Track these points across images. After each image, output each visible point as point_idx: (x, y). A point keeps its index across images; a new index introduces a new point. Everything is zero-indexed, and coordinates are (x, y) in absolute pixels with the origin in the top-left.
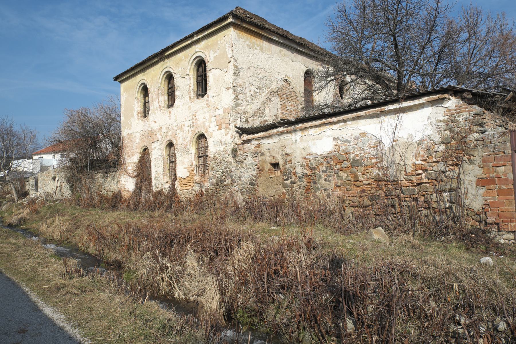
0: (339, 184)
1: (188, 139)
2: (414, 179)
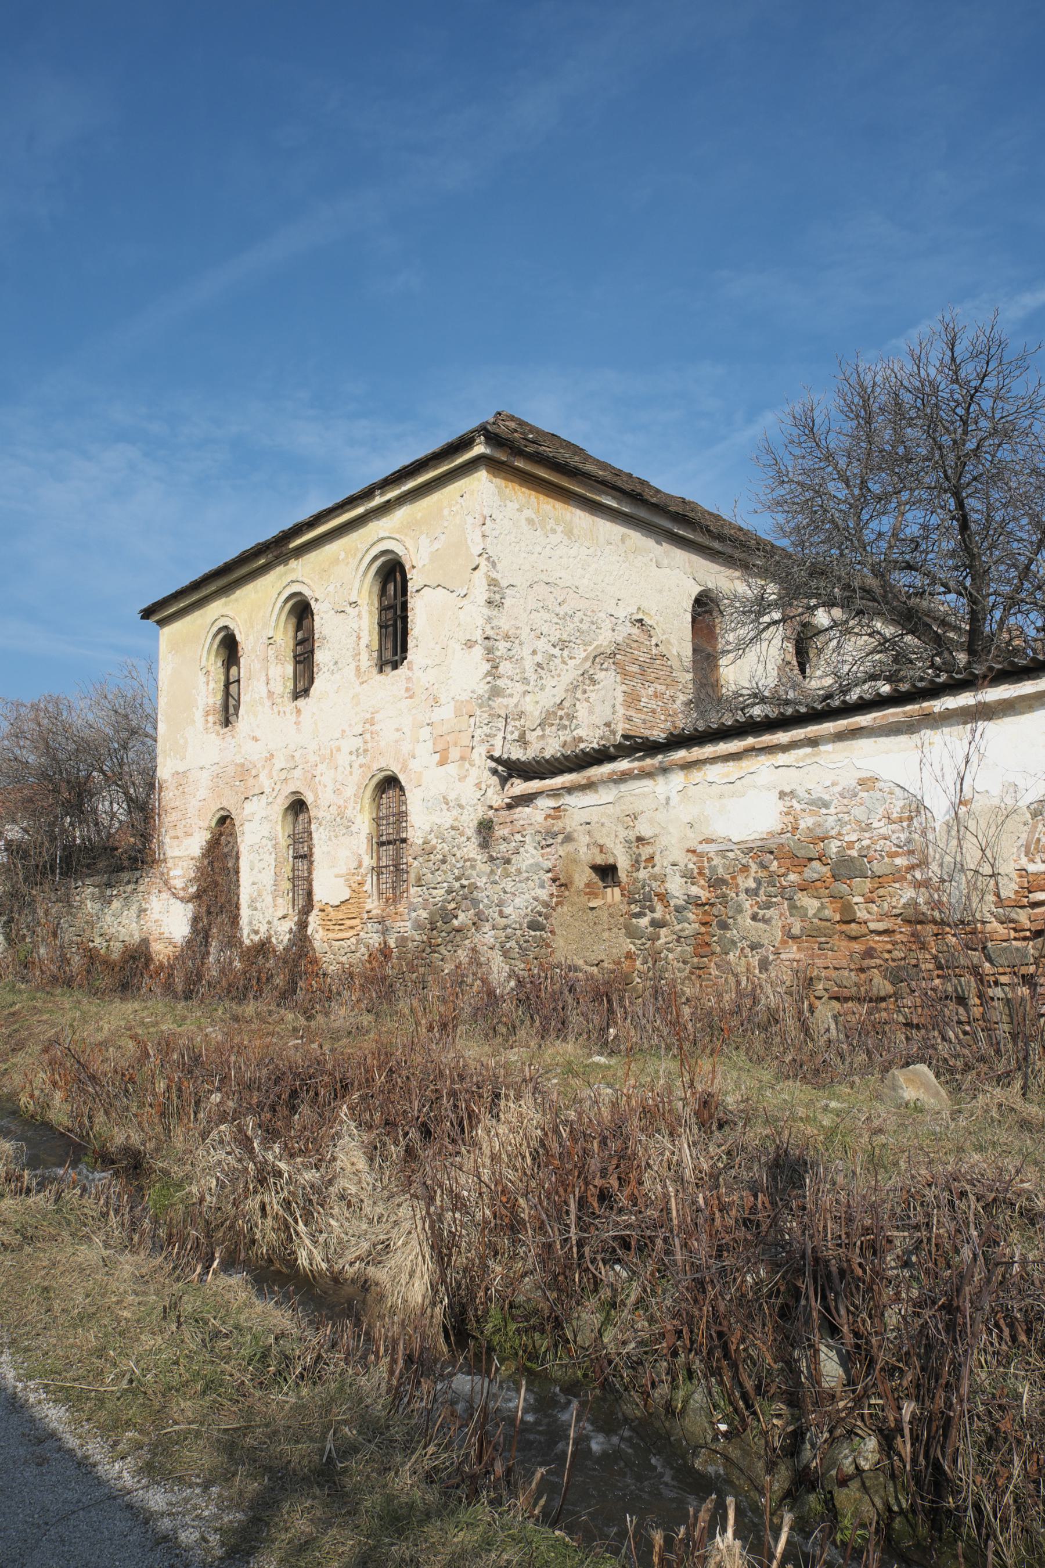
1: (349, 792)
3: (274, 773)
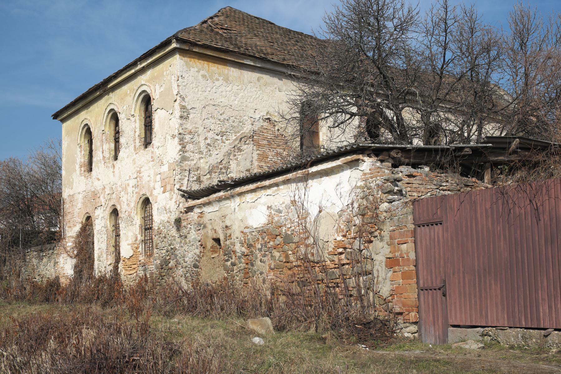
0: (272, 266)
1: (132, 205)
2: (336, 258)
3: (106, 196)
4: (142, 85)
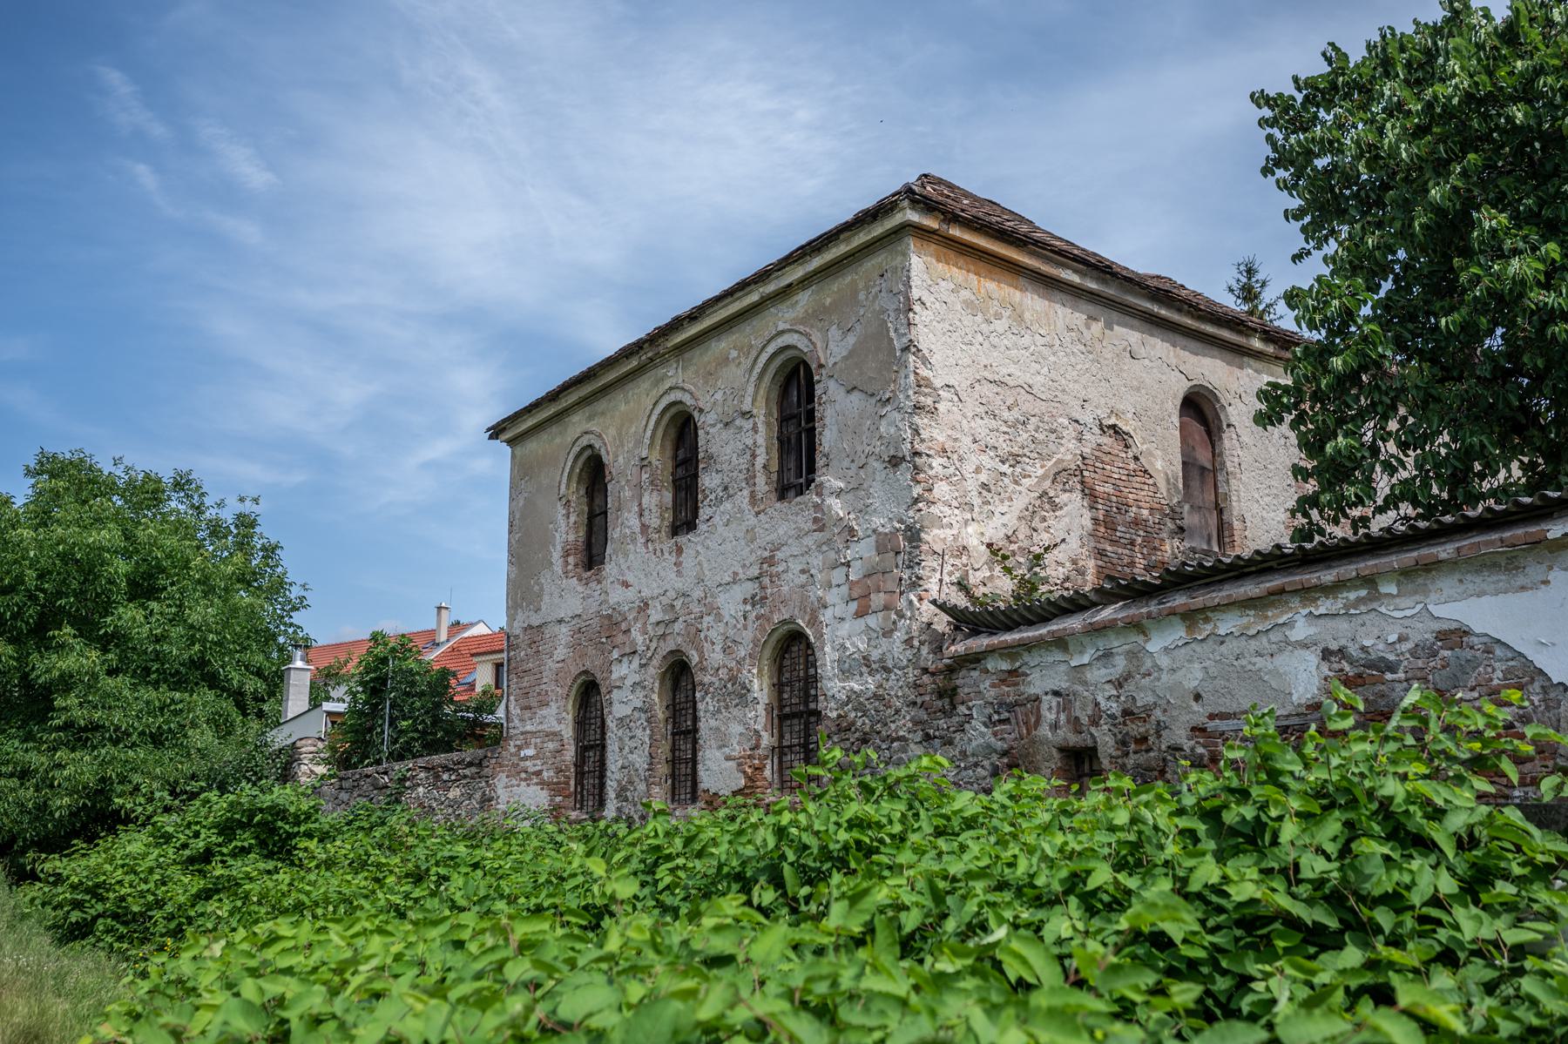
3: (650, 628)
4: (783, 332)
